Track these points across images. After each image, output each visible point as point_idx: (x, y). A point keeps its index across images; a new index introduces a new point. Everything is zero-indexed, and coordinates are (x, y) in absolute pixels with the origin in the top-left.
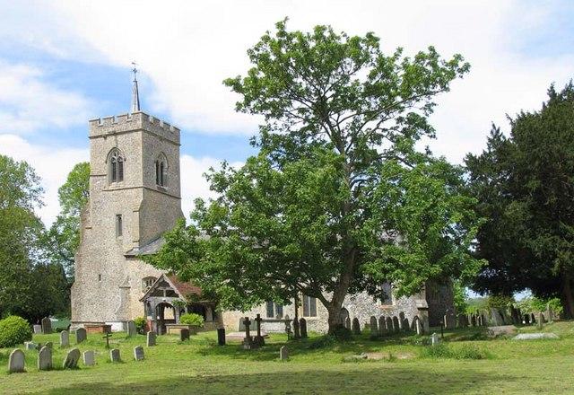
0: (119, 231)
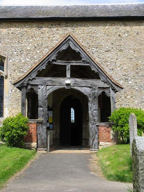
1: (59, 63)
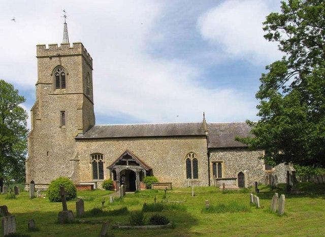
0: (63, 122)
1: (124, 160)
